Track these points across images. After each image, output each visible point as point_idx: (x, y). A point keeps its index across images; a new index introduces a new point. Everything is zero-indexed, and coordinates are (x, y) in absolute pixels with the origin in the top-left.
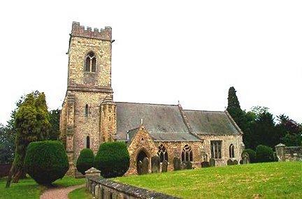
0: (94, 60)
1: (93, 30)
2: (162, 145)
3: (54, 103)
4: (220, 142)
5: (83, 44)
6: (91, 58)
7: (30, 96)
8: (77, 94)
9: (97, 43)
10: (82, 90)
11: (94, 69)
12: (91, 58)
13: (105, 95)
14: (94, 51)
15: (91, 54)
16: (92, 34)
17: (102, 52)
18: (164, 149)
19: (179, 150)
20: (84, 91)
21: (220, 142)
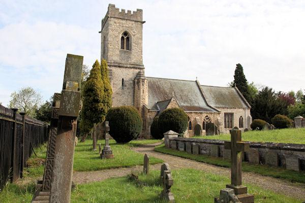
1: (126, 12)
5: (118, 24)
6: (125, 38)
7: (242, 68)
12: (125, 38)
13: (137, 71)
17: (134, 32)
19: (201, 120)
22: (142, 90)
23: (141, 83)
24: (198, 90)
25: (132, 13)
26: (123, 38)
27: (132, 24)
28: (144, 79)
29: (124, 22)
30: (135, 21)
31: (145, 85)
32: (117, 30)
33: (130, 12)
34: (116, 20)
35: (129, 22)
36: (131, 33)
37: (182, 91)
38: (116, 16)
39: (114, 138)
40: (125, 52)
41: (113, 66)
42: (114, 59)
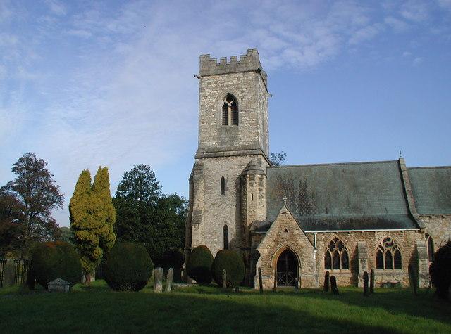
0: (235, 106)
1: (228, 61)
2: (336, 239)
3: (173, 184)
4: (398, 266)
5: (214, 85)
6: (229, 104)
7: (42, 163)
8: (206, 162)
9: (234, 79)
10: (215, 154)
11: (235, 121)
12: (229, 104)
13: (247, 160)
14: (231, 92)
15: (230, 97)
16: (227, 67)
17: (242, 92)
18: (341, 245)
19: (372, 246)
20: (216, 157)
21: (202, 165)
22: (249, 195)
23: (248, 182)
24: (398, 180)
25: (239, 60)
26: (225, 106)
27: (239, 79)
28: (254, 175)
29: (225, 77)
30: (244, 72)
31: (255, 185)
32: (213, 96)
33: (236, 58)
34: (211, 79)
35: (232, 75)
36: (237, 94)
37: (355, 186)
38: (211, 72)
39: (440, 250)
40: (227, 130)
41: (205, 157)
42: (208, 145)
